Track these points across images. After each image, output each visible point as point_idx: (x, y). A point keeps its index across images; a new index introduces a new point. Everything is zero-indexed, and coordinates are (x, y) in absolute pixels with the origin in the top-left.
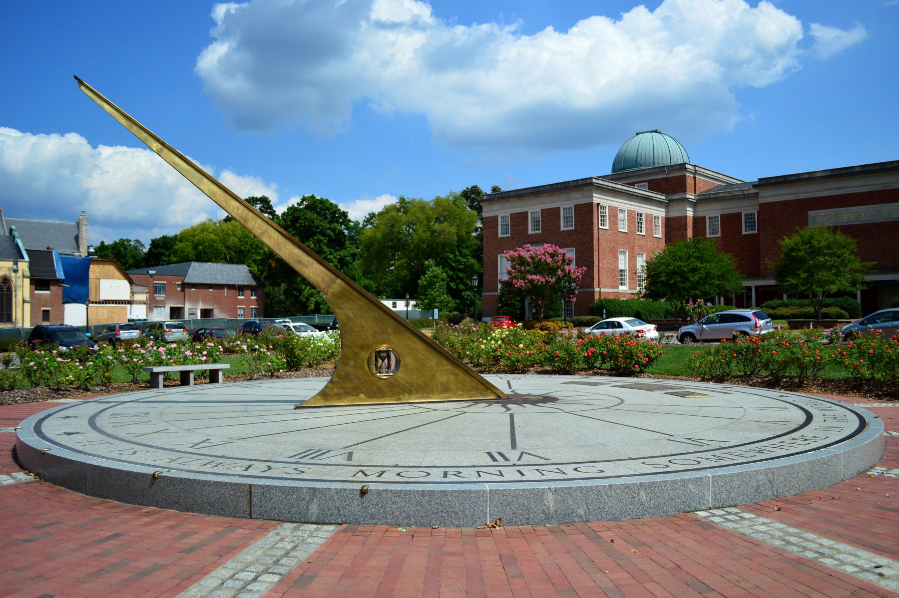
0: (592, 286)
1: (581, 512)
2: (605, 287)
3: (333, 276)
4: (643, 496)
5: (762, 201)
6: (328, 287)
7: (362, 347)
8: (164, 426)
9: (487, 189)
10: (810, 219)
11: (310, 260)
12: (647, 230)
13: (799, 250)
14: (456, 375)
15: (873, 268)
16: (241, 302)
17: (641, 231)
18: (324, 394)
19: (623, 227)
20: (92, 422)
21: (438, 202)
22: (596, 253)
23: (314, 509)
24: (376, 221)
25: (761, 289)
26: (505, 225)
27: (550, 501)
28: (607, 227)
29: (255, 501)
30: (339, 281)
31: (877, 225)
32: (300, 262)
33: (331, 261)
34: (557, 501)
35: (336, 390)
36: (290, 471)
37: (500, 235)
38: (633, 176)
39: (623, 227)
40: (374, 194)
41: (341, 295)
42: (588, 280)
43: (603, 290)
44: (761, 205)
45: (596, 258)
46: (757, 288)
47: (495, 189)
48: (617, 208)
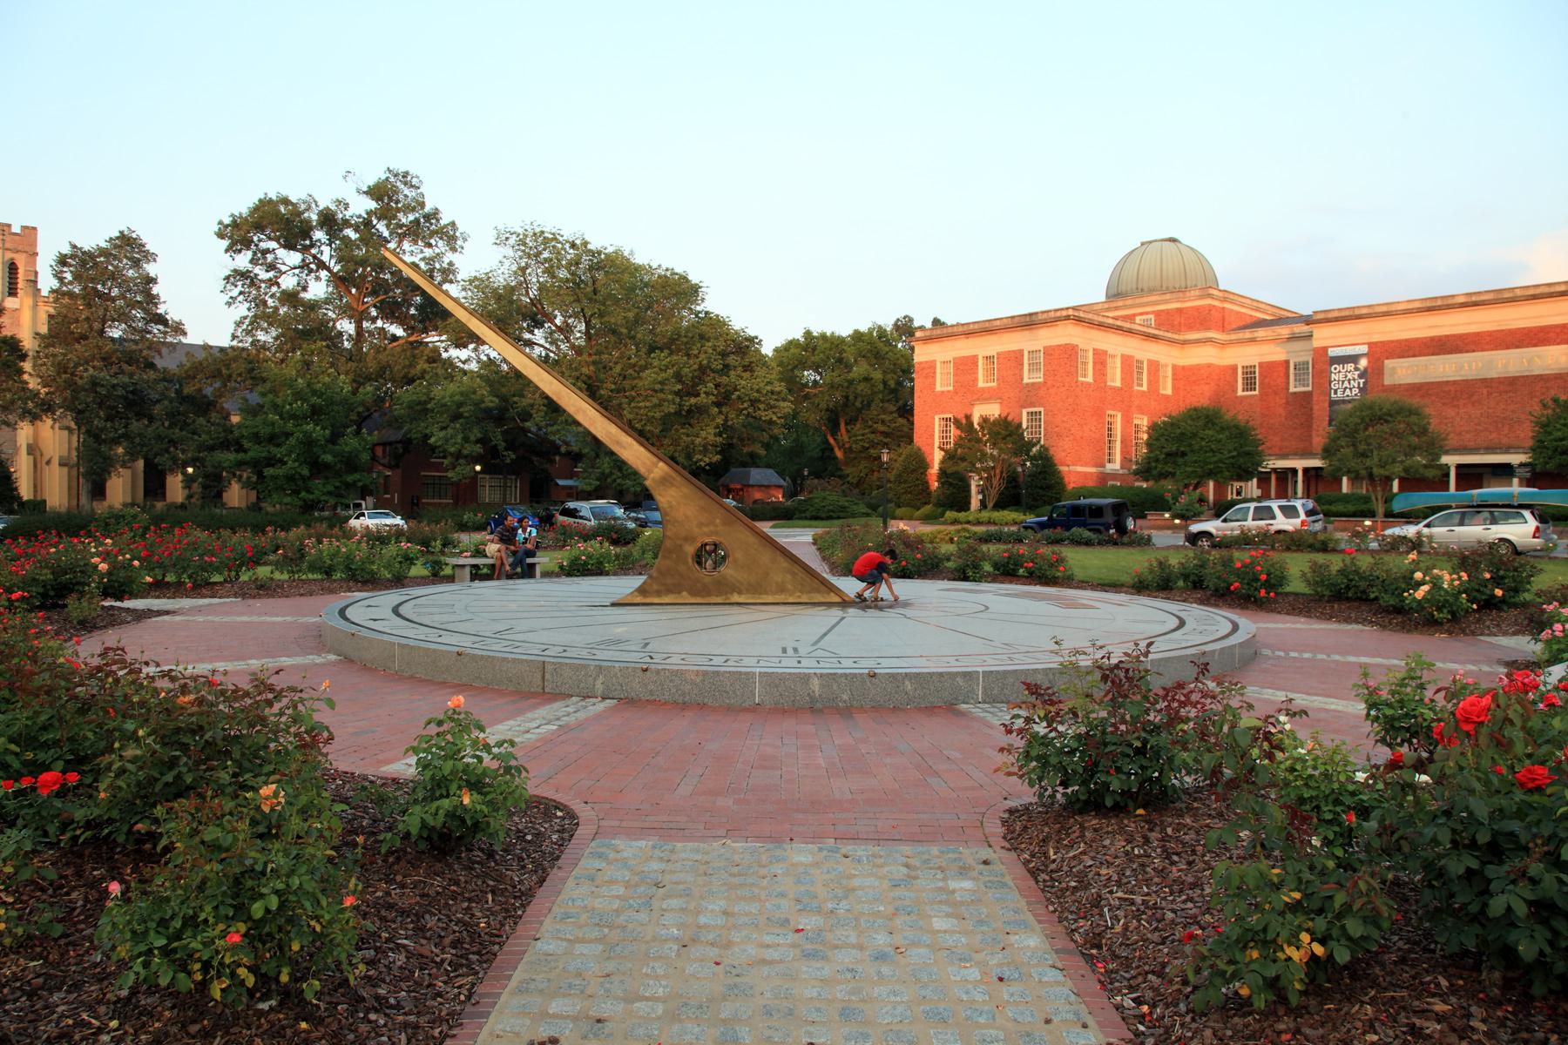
1: (845, 697)
3: (655, 459)
4: (908, 686)
6: (650, 471)
7: (686, 539)
8: (469, 616)
9: (922, 320)
10: (1386, 371)
11: (630, 440)
14: (794, 574)
16: (985, 396)
18: (642, 590)
19: (1115, 380)
20: (396, 610)
21: (858, 336)
23: (599, 687)
25: (1466, 470)
27: (816, 685)
28: (1090, 379)
29: (547, 676)
30: (661, 464)
31: (1486, 382)
32: (618, 443)
34: (822, 686)
35: (656, 587)
36: (584, 654)
37: (938, 388)
39: (1115, 380)
41: (664, 481)
47: (936, 322)
48: (1105, 352)
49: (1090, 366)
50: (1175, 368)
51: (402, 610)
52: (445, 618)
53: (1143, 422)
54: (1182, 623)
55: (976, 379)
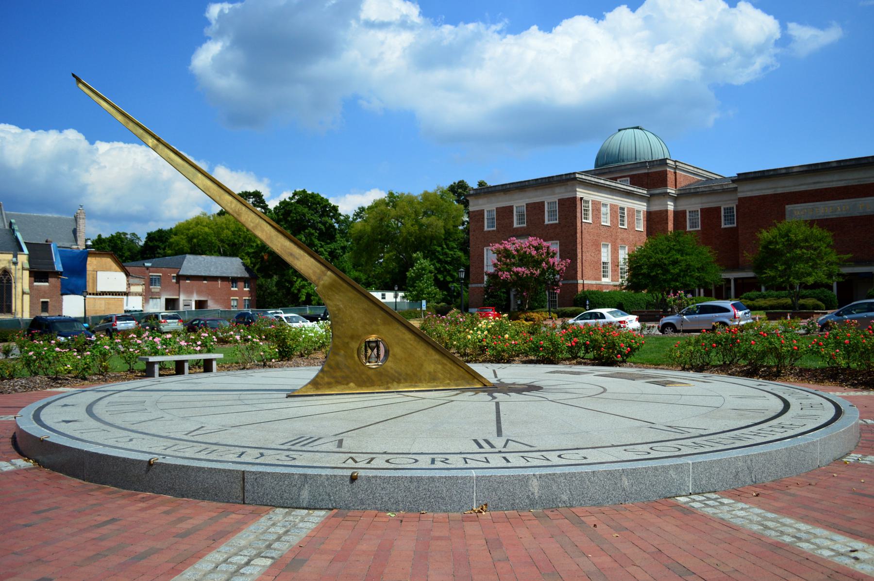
0: (575, 278)
1: (565, 497)
2: (589, 279)
3: (324, 269)
4: (626, 482)
5: (741, 195)
6: (319, 278)
7: (352, 338)
8: (159, 414)
9: (473, 184)
10: (787, 213)
11: (302, 252)
12: (629, 224)
13: (777, 243)
14: (444, 365)
15: (848, 260)
17: (623, 225)
18: (315, 383)
19: (606, 221)
20: (89, 410)
21: (426, 196)
22: (579, 246)
23: (305, 494)
24: (365, 215)
26: (491, 219)
27: (535, 487)
28: (590, 221)
30: (329, 273)
31: (853, 219)
33: (321, 254)
34: (541, 487)
35: (326, 379)
37: (486, 229)
38: (616, 172)
39: (606, 221)
40: (364, 189)
41: (331, 287)
42: (571, 273)
43: (586, 282)
44: (740, 199)
45: (579, 250)
46: (736, 280)
47: (481, 184)
49: (590, 212)
50: (153, 376)
51: (602, 390)
52: (137, 417)
53: (623, 255)
54: (787, 406)
55: (513, 222)
